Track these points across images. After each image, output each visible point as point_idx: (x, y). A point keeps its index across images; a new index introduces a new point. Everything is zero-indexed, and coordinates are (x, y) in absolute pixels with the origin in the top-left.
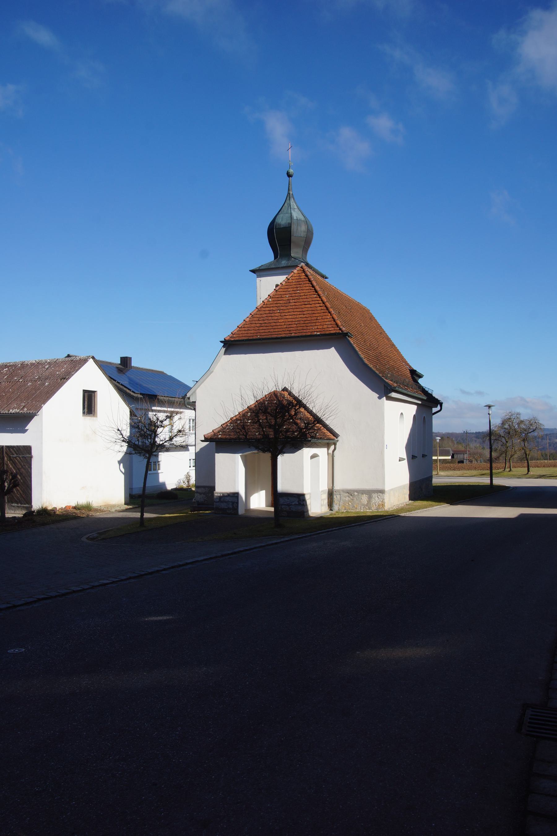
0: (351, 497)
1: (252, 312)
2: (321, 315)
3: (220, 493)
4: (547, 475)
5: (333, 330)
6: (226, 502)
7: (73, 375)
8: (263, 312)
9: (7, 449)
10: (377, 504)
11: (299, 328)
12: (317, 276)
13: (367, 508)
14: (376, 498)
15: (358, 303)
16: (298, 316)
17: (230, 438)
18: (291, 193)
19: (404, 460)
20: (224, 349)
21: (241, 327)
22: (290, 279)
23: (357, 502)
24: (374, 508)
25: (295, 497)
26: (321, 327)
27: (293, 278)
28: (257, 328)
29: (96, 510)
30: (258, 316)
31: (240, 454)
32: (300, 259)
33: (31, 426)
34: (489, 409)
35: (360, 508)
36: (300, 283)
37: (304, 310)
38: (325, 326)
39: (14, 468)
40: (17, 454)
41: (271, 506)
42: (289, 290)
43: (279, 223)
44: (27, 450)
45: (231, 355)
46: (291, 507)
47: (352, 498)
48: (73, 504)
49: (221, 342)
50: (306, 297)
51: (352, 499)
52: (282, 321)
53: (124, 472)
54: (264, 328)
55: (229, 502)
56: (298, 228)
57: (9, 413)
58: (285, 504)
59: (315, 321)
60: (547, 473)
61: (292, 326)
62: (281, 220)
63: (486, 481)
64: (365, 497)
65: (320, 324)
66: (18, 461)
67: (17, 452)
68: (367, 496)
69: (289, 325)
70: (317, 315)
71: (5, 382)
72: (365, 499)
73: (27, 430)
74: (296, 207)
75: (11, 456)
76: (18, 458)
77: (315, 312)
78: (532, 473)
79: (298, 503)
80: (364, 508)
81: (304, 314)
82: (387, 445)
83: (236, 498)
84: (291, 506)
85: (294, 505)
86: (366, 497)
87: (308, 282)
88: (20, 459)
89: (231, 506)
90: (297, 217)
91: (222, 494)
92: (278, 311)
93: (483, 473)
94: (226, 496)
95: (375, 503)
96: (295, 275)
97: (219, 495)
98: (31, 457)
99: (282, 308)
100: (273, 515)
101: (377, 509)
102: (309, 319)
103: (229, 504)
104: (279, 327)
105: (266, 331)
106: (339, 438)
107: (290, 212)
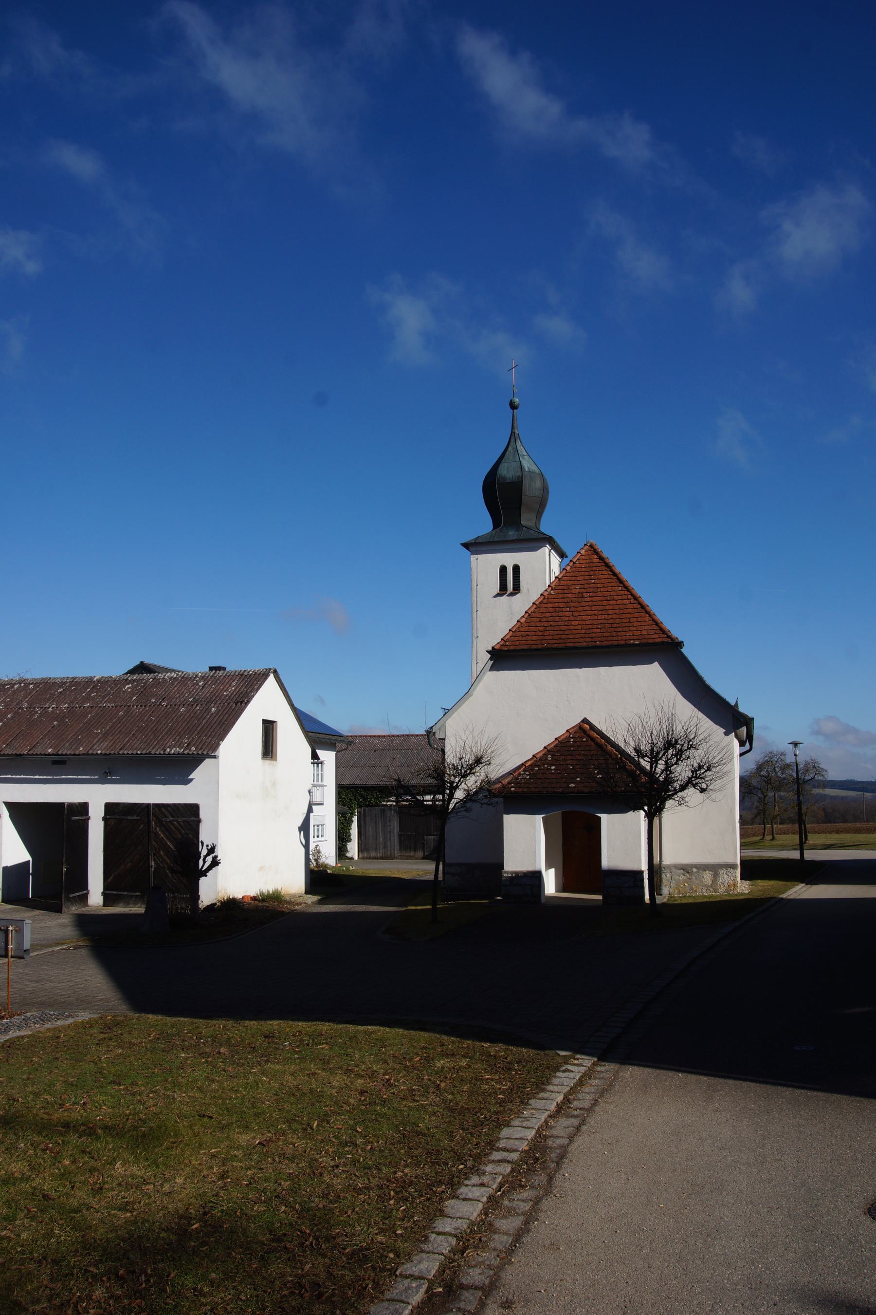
0: (687, 875)
1: (529, 609)
2: (636, 615)
3: (512, 873)
4: (837, 844)
5: (658, 638)
7: (253, 696)
8: (545, 610)
9: (156, 810)
10: (726, 884)
11: (605, 634)
13: (712, 889)
14: (725, 876)
16: (599, 617)
18: (516, 432)
20: (491, 663)
21: (515, 631)
23: (697, 882)
24: (722, 890)
26: (638, 633)
27: (581, 561)
28: (540, 633)
29: (289, 903)
30: (538, 615)
31: (543, 815)
33: (198, 774)
34: (795, 747)
35: (700, 891)
36: (594, 569)
37: (607, 607)
38: (644, 632)
39: (167, 837)
40: (173, 816)
42: (578, 578)
43: (503, 475)
44: (194, 809)
45: (501, 672)
48: (252, 893)
49: (487, 651)
50: (606, 589)
51: (689, 879)
52: (577, 623)
53: (304, 844)
54: (552, 633)
57: (167, 753)
59: (627, 625)
60: (837, 842)
61: (595, 630)
62: (506, 471)
63: (795, 855)
65: (635, 628)
66: (175, 827)
67: (174, 814)
68: (711, 873)
69: (589, 629)
70: (629, 616)
71: (137, 706)
72: (707, 877)
73: (192, 780)
74: (525, 453)
75: (163, 819)
76: (175, 822)
77: (626, 611)
78: (811, 842)
81: (608, 614)
87: (604, 568)
88: (180, 825)
90: (529, 468)
92: (568, 609)
93: (829, 842)
94: (521, 877)
95: (723, 883)
96: (584, 557)
98: (199, 821)
99: (572, 604)
100: (601, 903)
101: (727, 891)
102: (618, 621)
104: (574, 632)
105: (555, 637)
107: (518, 460)
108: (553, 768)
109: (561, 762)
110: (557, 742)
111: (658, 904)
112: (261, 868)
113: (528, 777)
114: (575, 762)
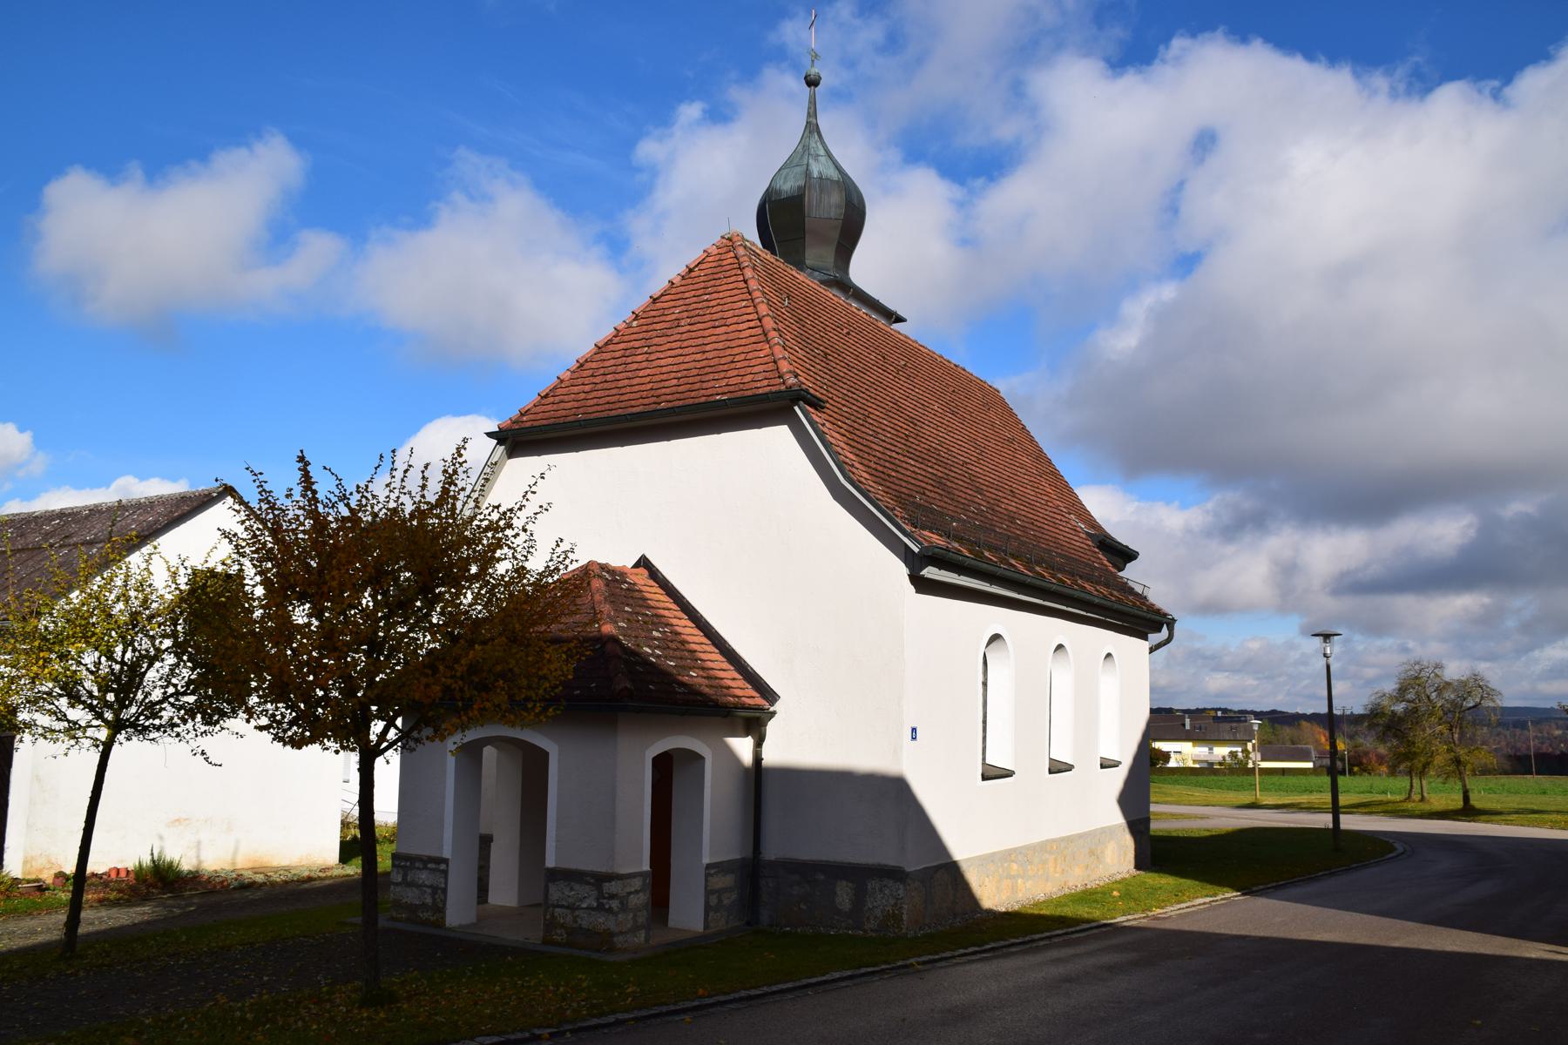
6: (419, 886)
12: (788, 270)
15: (956, 366)
19: (1117, 766)
22: (697, 269)
32: (828, 270)
49: (490, 435)
56: (821, 197)
58: (564, 903)
63: (1324, 820)
68: (850, 885)
74: (822, 152)
82: (914, 730)
83: (443, 875)
84: (577, 913)
85: (587, 908)
103: (425, 892)
106: (777, 707)
112: (178, 820)
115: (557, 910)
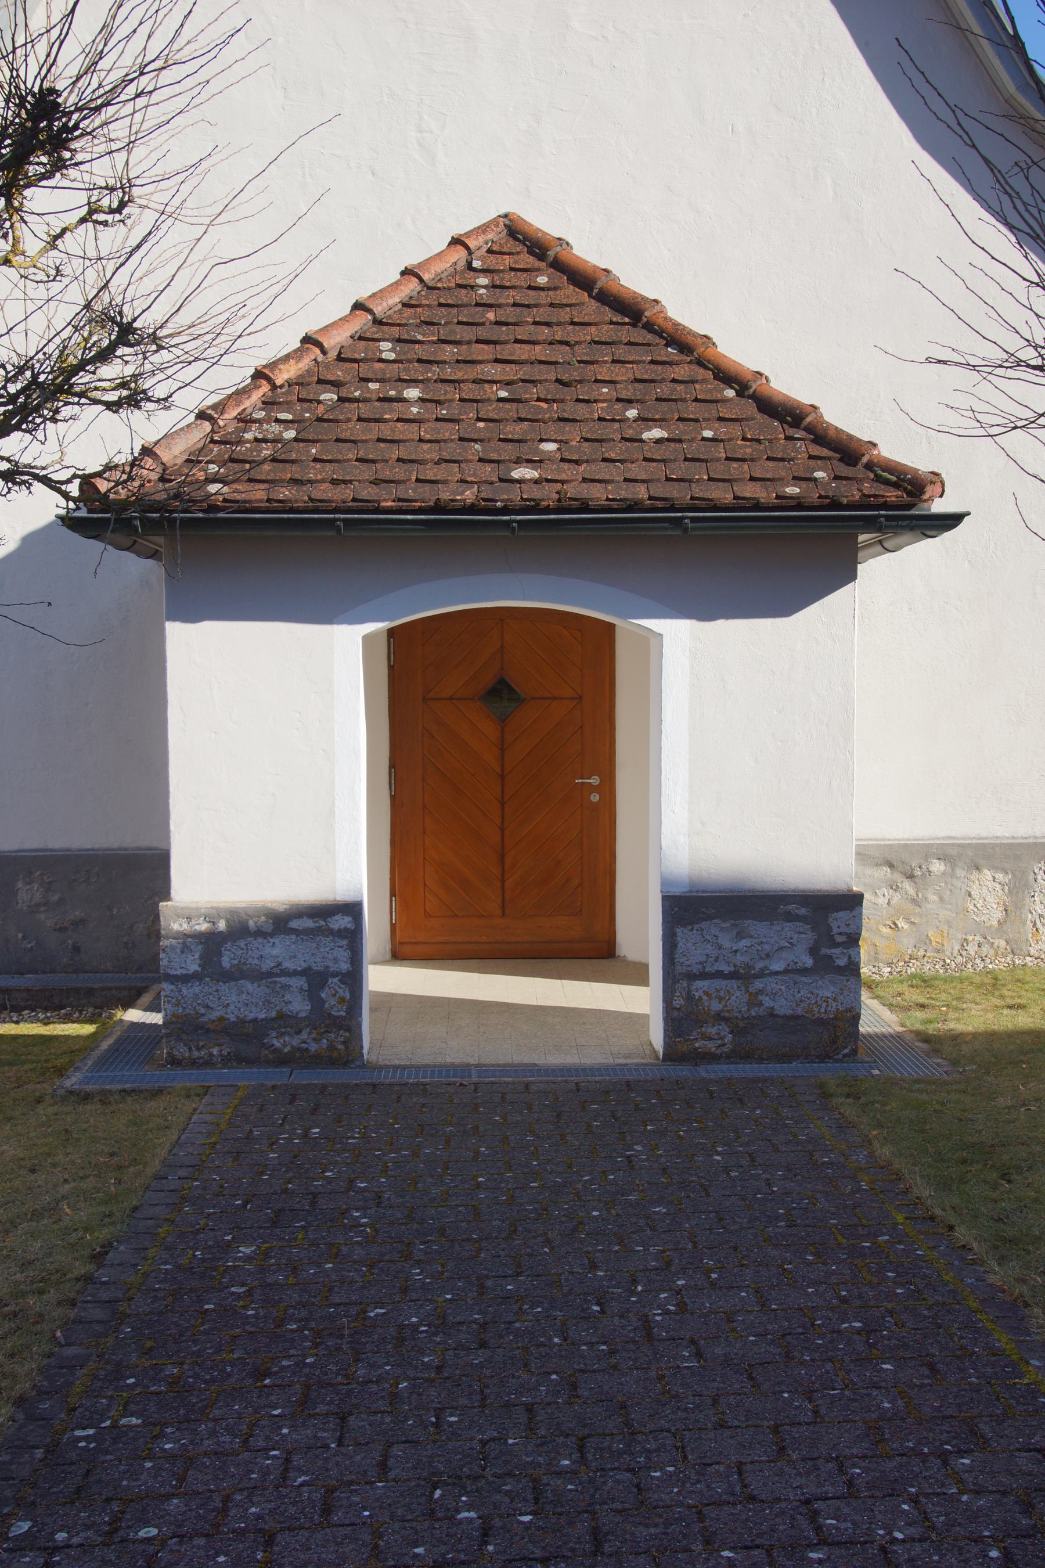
0: (908, 886)
6: (259, 976)
13: (1002, 943)
17: (311, 499)
25: (790, 917)
35: (957, 947)
41: (388, 956)
46: (761, 992)
47: (911, 891)
51: (914, 901)
55: (285, 973)
64: (990, 884)
68: (1000, 876)
79: (809, 962)
80: (985, 949)
84: (758, 984)
85: (786, 971)
86: (998, 887)
89: (299, 1006)
91: (227, 921)
97: (204, 927)
103: (286, 987)
108: (413, 393)
109: (448, 373)
110: (412, 286)
111: (869, 1036)
113: (290, 434)
114: (510, 372)
115: (699, 983)
